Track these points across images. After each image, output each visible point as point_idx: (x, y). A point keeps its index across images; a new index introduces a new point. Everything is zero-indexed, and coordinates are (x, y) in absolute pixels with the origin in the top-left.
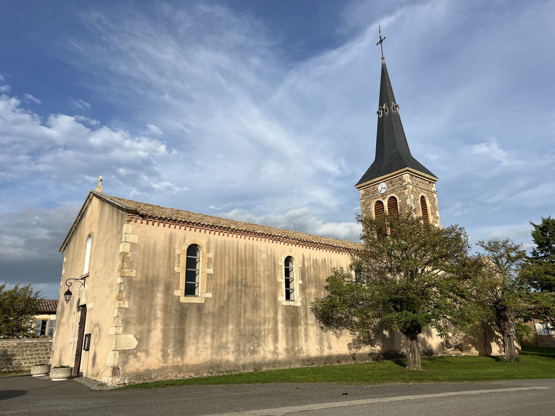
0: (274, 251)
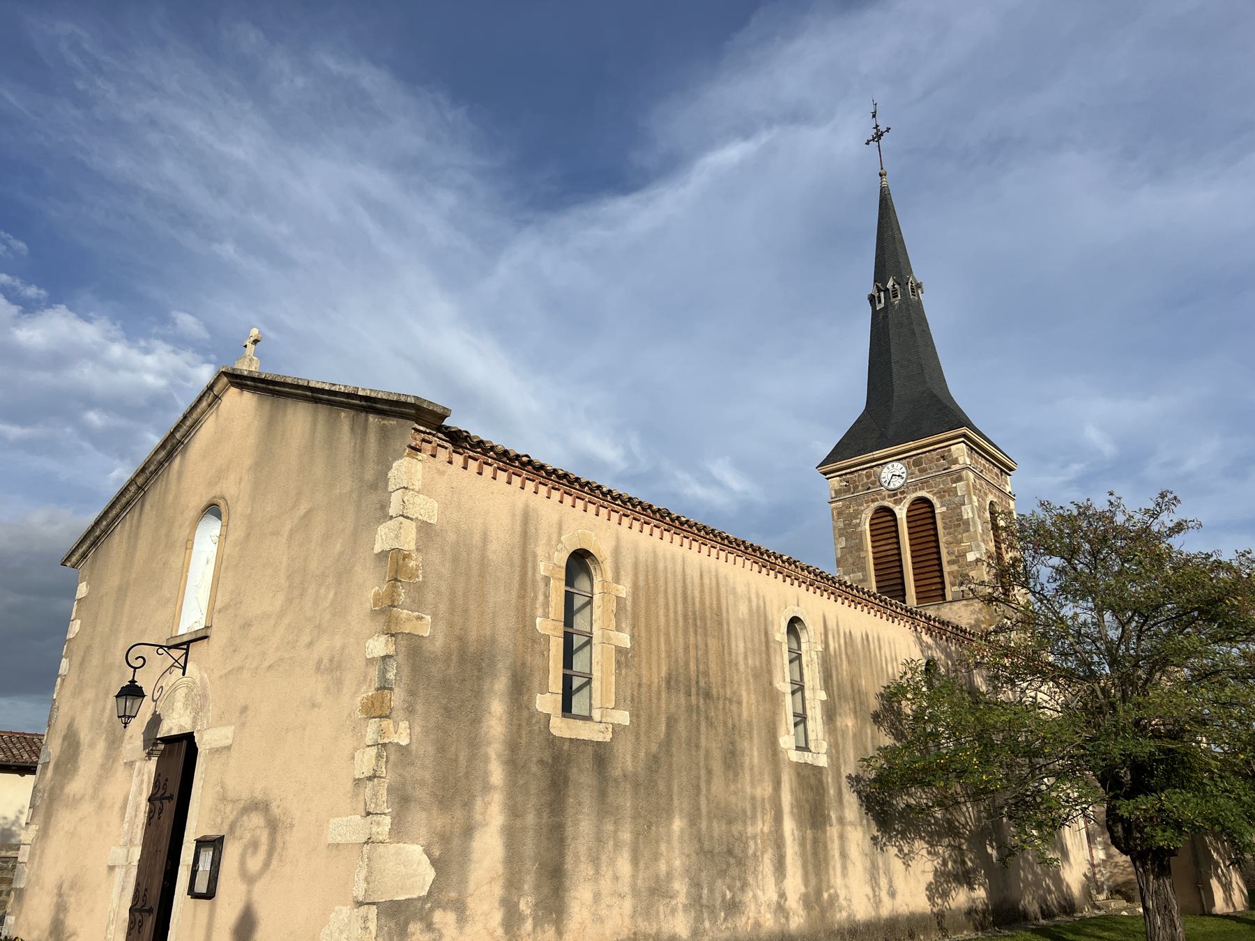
0: (764, 598)
